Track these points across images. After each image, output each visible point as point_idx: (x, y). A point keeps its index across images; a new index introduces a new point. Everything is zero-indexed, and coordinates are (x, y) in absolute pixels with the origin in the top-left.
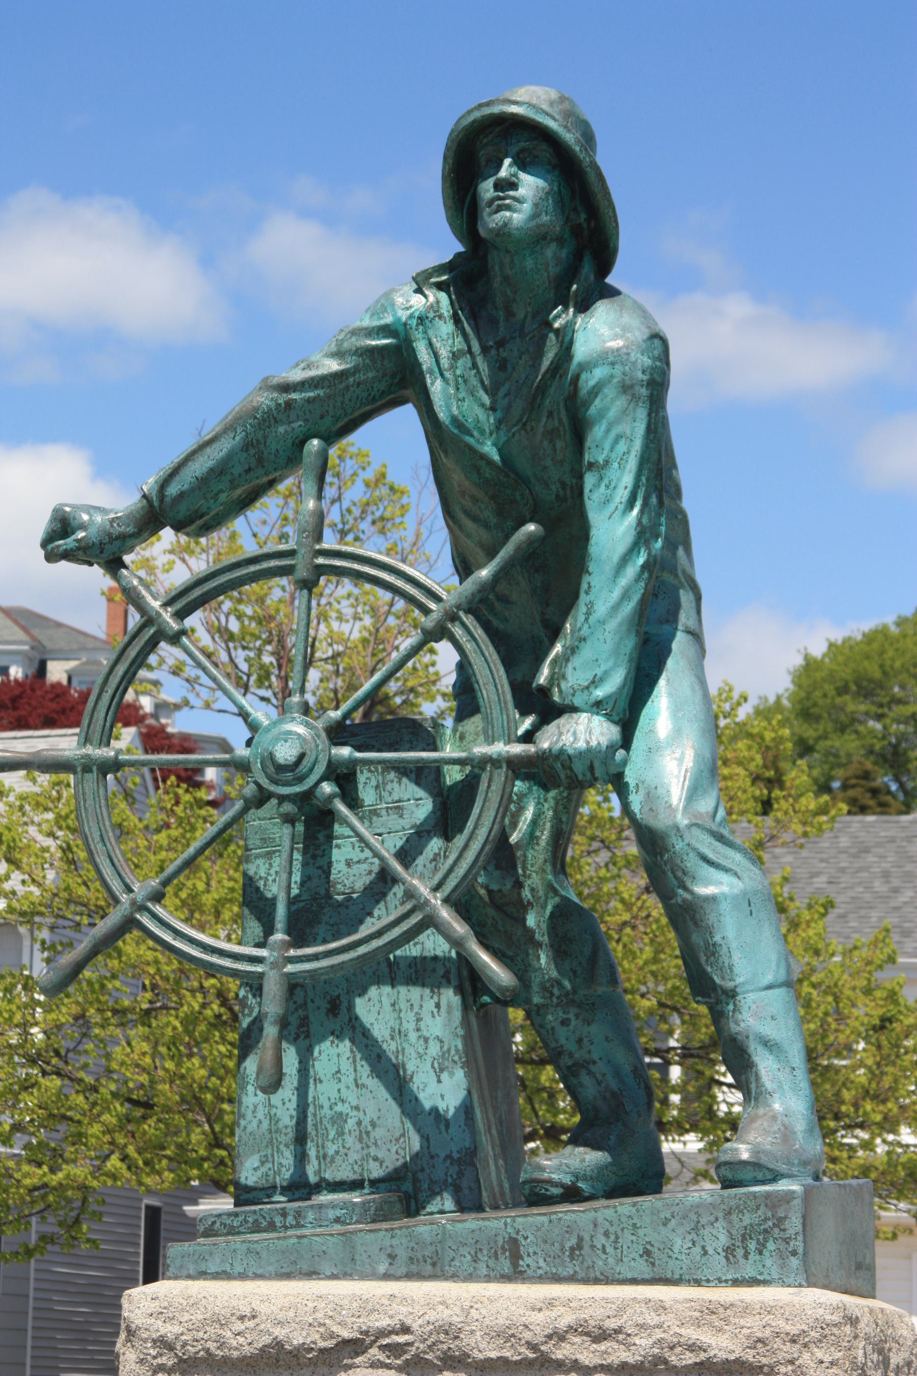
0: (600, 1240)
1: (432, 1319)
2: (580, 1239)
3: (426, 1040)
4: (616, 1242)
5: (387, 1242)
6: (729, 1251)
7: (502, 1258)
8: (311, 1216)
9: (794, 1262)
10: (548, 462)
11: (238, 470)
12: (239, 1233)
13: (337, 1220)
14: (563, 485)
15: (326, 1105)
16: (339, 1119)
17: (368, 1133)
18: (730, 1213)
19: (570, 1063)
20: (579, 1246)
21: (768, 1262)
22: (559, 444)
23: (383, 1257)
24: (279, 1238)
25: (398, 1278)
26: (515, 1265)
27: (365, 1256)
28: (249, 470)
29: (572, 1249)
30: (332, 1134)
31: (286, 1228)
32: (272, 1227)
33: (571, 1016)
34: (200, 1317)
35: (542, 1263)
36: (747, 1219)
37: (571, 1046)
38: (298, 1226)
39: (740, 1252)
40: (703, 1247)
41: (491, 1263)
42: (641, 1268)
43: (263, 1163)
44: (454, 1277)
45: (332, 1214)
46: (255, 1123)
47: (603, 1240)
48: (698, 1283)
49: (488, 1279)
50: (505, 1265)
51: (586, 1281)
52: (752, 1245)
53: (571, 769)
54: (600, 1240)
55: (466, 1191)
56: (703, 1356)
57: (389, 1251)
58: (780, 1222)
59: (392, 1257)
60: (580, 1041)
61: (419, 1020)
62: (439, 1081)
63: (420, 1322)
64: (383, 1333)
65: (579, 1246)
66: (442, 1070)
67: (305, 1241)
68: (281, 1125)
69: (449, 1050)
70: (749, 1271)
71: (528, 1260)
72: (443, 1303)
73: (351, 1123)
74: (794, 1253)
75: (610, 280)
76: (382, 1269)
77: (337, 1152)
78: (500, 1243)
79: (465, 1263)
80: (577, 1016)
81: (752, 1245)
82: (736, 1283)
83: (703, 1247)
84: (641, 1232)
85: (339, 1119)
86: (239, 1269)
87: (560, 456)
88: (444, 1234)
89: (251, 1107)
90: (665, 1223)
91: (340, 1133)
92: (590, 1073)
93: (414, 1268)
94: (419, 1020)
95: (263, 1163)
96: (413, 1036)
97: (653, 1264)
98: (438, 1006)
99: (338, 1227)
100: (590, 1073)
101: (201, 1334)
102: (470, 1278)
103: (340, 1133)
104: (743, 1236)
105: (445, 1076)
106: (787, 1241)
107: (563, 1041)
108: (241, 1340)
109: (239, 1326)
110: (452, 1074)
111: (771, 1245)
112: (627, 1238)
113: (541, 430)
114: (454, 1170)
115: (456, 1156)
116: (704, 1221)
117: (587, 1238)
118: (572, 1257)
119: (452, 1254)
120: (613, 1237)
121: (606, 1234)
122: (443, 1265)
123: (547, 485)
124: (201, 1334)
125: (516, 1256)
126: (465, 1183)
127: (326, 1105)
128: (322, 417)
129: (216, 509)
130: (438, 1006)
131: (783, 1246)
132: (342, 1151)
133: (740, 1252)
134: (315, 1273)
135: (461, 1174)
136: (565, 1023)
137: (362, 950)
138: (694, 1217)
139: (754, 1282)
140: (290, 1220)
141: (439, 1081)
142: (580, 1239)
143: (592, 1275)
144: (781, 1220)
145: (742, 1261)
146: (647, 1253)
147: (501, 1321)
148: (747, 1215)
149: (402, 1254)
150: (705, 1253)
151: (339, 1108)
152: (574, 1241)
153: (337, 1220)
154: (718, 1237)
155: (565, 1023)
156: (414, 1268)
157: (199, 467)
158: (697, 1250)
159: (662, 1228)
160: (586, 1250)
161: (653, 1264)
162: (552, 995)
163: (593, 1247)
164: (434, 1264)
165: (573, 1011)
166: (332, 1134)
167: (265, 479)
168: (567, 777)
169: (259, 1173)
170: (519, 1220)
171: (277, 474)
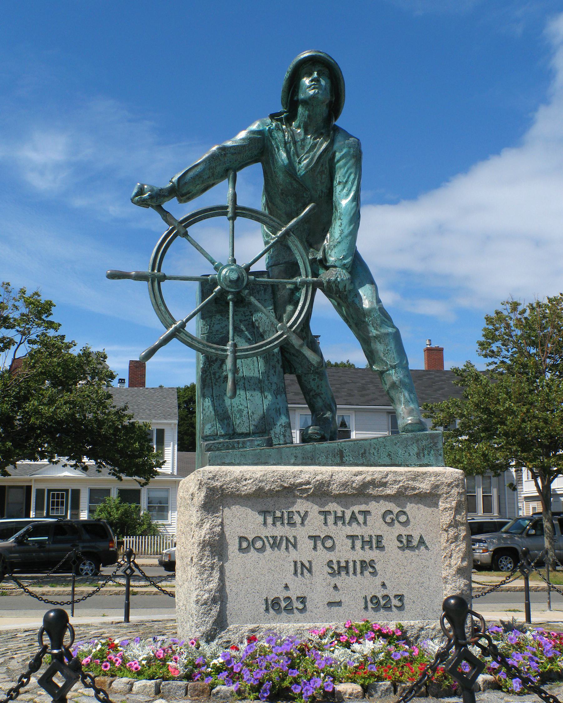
0: (372, 451)
1: (319, 479)
2: (365, 450)
3: (271, 384)
4: (378, 451)
5: (294, 451)
6: (418, 454)
7: (337, 457)
8: (248, 444)
9: (441, 458)
10: (319, 183)
11: (206, 177)
12: (221, 450)
13: (258, 445)
14: (322, 192)
15: (236, 406)
16: (240, 411)
17: (251, 416)
18: (418, 441)
19: (314, 394)
20: (365, 453)
21: (432, 458)
22: (324, 176)
23: (293, 457)
24: (253, 450)
25: (298, 465)
26: (342, 460)
27: (285, 457)
28: (209, 177)
29: (362, 454)
30: (238, 416)
31: (239, 448)
32: (233, 448)
33: (316, 378)
34: (229, 479)
35: (351, 459)
36: (424, 443)
37: (315, 388)
38: (243, 447)
39: (422, 455)
40: (409, 453)
41: (333, 459)
42: (387, 460)
43: (212, 427)
44: (319, 464)
45: (256, 443)
46: (209, 412)
47: (373, 450)
48: (407, 466)
49: (332, 465)
50: (338, 460)
51: (367, 466)
52: (426, 452)
53: (338, 287)
54: (372, 451)
55: (288, 437)
56: (417, 491)
57: (295, 455)
58: (435, 444)
59: (296, 457)
60: (318, 386)
61: (268, 376)
62: (277, 398)
63: (314, 480)
64: (301, 484)
65: (365, 453)
66: (277, 394)
67: (263, 451)
68: (219, 413)
69: (279, 387)
70: (426, 462)
71: (347, 458)
72: (321, 473)
73: (245, 413)
74: (440, 455)
75: (339, 122)
76: (292, 461)
77: (240, 423)
78: (336, 451)
79: (323, 459)
80: (318, 377)
81: (426, 452)
82: (421, 466)
83: (409, 453)
84: (387, 448)
85: (240, 411)
86: (238, 461)
87: (323, 181)
88: (315, 448)
89: (207, 407)
90: (396, 444)
91: (241, 416)
92: (321, 397)
93: (304, 461)
94: (268, 376)
95: (212, 427)
96: (266, 382)
97: (391, 459)
98: (275, 372)
99: (259, 448)
100: (321, 397)
101: (229, 486)
102: (325, 464)
103: (241, 416)
104: (423, 449)
105: (279, 396)
106: (438, 450)
107: (313, 386)
108: (245, 488)
109: (245, 483)
110: (281, 396)
111: (432, 452)
112: (382, 449)
113: (318, 170)
114: (283, 430)
115: (283, 424)
116: (409, 444)
117: (367, 450)
118: (362, 457)
119: (318, 456)
120: (377, 450)
121: (374, 448)
122: (315, 460)
123: (316, 191)
124: (229, 486)
125: (342, 456)
126: (287, 434)
127: (236, 406)
128: (236, 161)
129: (195, 191)
130: (275, 372)
131: (437, 452)
132: (242, 423)
133: (422, 455)
134: (267, 463)
135: (285, 431)
136: (314, 380)
137: (264, 348)
138: (405, 442)
139: (427, 465)
140: (240, 445)
141: (277, 398)
142: (365, 450)
143: (370, 463)
144: (436, 443)
145: (422, 458)
146: (389, 455)
147: (344, 479)
148: (424, 442)
149: (300, 456)
150: (410, 455)
151: (240, 407)
152: (363, 451)
153: (258, 445)
154: (414, 449)
155: (314, 380)
156: (304, 461)
157: (191, 174)
158: (407, 454)
159: (394, 446)
160: (367, 454)
161: (391, 459)
162: (311, 370)
163: (370, 453)
164: (312, 460)
165: (317, 376)
166: (238, 416)
167: (213, 182)
168: (336, 289)
169: (211, 430)
170: (343, 443)
171: (216, 181)
